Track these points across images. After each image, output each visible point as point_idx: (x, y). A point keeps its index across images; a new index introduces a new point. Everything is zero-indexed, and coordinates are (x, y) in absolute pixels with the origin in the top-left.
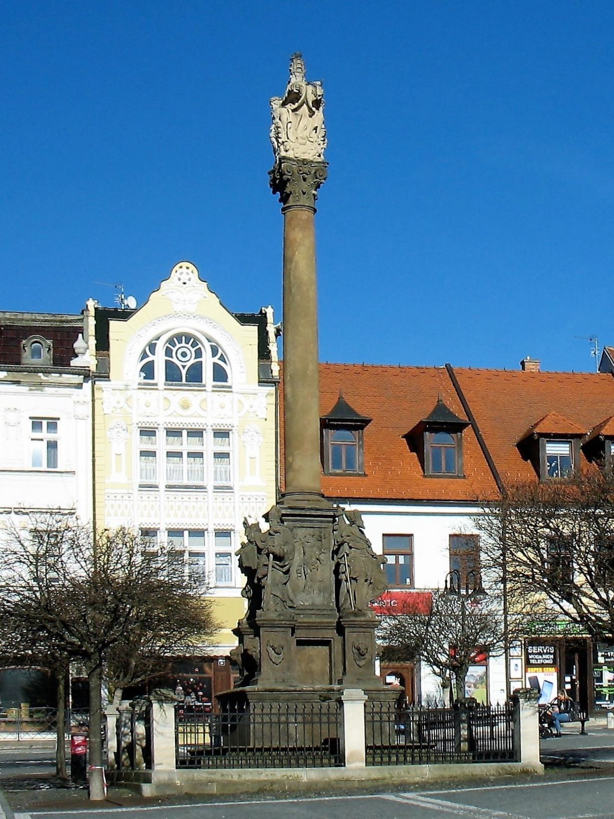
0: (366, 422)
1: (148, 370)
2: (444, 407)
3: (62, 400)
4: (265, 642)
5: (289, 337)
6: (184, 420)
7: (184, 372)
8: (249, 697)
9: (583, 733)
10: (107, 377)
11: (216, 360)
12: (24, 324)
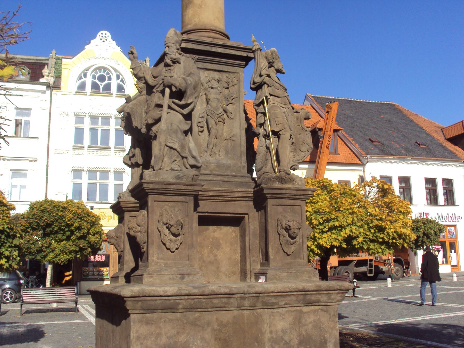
1: (82, 87)
3: (31, 96)
4: (156, 217)
7: (101, 87)
8: (129, 305)
10: (59, 88)
11: (119, 81)
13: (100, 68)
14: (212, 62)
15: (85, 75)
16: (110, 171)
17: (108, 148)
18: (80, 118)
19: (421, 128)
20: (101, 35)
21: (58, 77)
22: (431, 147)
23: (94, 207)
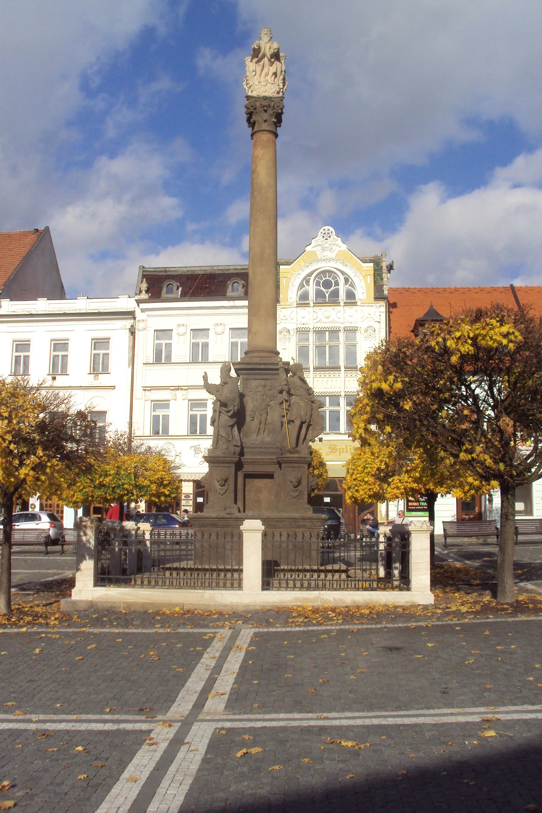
1: (304, 297)
6: (326, 325)
7: (327, 295)
12: (230, 272)
13: (324, 272)
14: (259, 374)
15: (308, 282)
16: (340, 395)
17: (338, 368)
20: (323, 232)
23: (324, 439)
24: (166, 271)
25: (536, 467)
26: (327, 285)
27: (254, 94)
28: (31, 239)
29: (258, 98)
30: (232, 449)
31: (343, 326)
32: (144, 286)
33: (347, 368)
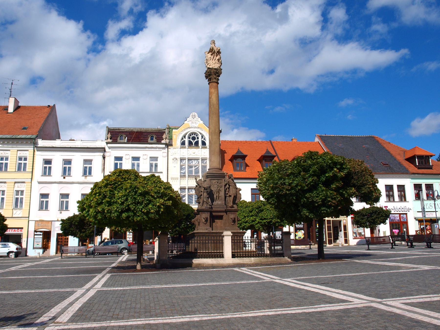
0: (246, 156)
1: (183, 143)
2: (269, 151)
5: (217, 130)
7: (194, 143)
9: (310, 249)
10: (172, 145)
13: (192, 133)
18: (182, 160)
19: (389, 152)
21: (171, 139)
22: (391, 166)
24: (119, 129)
25: (368, 206)
26: (194, 138)
27: (211, 67)
28: (47, 110)
29: (212, 69)
30: (209, 206)
31: (201, 157)
32: (109, 135)
33: (189, 176)
